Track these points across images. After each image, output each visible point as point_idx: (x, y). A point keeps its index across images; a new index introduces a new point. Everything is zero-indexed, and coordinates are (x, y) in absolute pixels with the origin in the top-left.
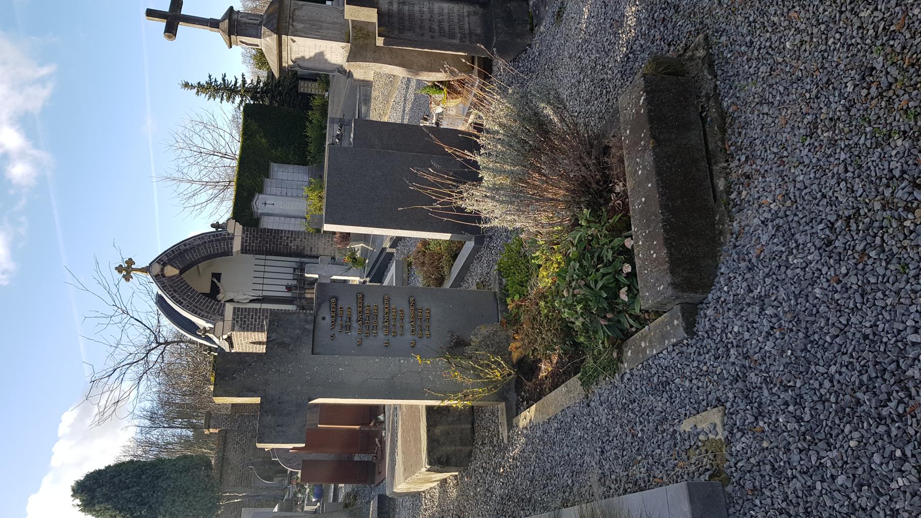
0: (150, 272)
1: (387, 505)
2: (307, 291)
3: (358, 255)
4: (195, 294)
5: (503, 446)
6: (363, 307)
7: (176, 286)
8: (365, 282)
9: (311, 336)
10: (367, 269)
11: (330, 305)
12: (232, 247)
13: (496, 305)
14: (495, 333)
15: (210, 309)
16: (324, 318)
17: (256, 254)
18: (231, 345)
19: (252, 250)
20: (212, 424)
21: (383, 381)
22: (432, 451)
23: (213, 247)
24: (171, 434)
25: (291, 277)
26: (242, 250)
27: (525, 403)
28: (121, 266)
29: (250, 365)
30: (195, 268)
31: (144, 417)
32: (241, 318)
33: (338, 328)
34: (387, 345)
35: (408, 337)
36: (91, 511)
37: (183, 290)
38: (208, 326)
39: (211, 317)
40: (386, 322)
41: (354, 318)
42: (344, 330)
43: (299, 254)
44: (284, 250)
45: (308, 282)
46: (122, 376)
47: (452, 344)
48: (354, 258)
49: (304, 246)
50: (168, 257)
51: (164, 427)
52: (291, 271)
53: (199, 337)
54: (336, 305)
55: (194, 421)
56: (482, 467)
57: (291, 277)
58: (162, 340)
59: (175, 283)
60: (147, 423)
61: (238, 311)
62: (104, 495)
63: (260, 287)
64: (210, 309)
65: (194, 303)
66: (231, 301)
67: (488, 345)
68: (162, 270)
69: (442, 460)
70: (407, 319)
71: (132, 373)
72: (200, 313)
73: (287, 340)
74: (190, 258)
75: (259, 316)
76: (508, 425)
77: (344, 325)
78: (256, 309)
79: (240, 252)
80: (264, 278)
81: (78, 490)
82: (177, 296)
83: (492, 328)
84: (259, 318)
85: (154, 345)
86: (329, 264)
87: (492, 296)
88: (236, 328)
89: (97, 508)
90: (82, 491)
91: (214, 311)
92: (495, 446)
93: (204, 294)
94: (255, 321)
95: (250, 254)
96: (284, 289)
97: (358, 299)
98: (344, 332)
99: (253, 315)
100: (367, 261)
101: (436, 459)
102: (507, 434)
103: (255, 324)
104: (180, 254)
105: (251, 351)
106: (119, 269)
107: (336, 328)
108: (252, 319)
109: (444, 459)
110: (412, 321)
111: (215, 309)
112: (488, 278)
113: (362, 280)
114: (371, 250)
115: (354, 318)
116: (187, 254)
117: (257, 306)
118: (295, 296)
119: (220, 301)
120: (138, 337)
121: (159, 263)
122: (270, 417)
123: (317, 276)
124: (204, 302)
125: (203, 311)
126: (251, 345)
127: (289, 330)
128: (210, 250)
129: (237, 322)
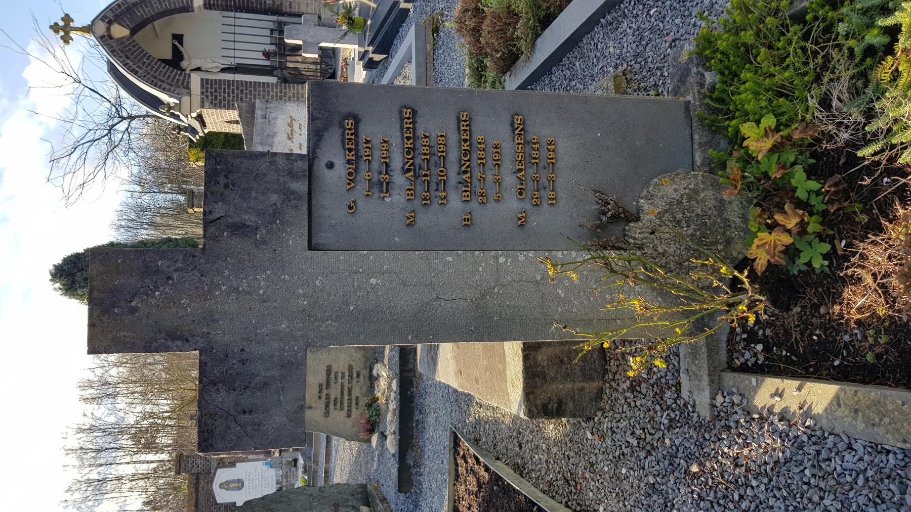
0: (93, 33)
1: (411, 361)
2: (289, 58)
5: (695, 419)
6: (415, 138)
8: (366, 52)
9: (305, 208)
10: (369, 35)
11: (343, 135)
13: (688, 132)
15: (172, 81)
16: (330, 166)
17: (223, 10)
18: (203, 124)
19: (218, 4)
24: (164, 199)
25: (268, 40)
26: (205, 4)
27: (760, 347)
28: (56, 24)
29: (169, 278)
30: (149, 27)
31: (133, 182)
32: (211, 93)
33: (362, 187)
34: (468, 223)
35: (512, 204)
36: (74, 295)
37: (137, 56)
38: (172, 101)
39: (174, 90)
40: (465, 172)
41: (397, 162)
42: (376, 190)
43: (275, 11)
45: (288, 48)
46: (84, 156)
47: (604, 219)
48: (350, 19)
50: (113, 12)
52: (268, 33)
53: (164, 114)
54: (356, 134)
55: (184, 186)
56: (633, 433)
57: (268, 40)
58: (125, 114)
59: (125, 47)
60: (138, 188)
61: (207, 84)
63: (231, 53)
64: (172, 81)
65: (152, 73)
66: (198, 69)
67: (679, 222)
68: (108, 29)
70: (508, 165)
71: (95, 152)
72: (161, 85)
73: (250, 218)
75: (233, 89)
76: (712, 382)
77: (375, 179)
78: (229, 81)
79: (202, 8)
80: (235, 26)
81: (56, 274)
82: (131, 64)
83: (685, 183)
84: (233, 92)
85: (116, 120)
86: (315, 25)
87: (683, 110)
88: (207, 104)
89: (79, 292)
90: (61, 276)
92: (668, 408)
93: (163, 61)
94: (229, 96)
95: (215, 9)
96: (260, 56)
97: (402, 120)
98: (376, 195)
99: (225, 89)
100: (369, 22)
102: (708, 401)
103: (229, 100)
104: (128, 9)
106: (55, 28)
107: (358, 187)
108: (224, 93)
110: (520, 170)
111: (178, 80)
112: (637, 66)
113: (362, 50)
114: (373, 8)
115: (397, 162)
116: (137, 8)
117: (229, 77)
118: (274, 64)
119: (185, 70)
120: (100, 111)
121: (103, 21)
122: (223, 393)
123: (300, 42)
124: (164, 71)
125: (163, 82)
126: (227, 125)
128: (166, 5)
129: (207, 96)
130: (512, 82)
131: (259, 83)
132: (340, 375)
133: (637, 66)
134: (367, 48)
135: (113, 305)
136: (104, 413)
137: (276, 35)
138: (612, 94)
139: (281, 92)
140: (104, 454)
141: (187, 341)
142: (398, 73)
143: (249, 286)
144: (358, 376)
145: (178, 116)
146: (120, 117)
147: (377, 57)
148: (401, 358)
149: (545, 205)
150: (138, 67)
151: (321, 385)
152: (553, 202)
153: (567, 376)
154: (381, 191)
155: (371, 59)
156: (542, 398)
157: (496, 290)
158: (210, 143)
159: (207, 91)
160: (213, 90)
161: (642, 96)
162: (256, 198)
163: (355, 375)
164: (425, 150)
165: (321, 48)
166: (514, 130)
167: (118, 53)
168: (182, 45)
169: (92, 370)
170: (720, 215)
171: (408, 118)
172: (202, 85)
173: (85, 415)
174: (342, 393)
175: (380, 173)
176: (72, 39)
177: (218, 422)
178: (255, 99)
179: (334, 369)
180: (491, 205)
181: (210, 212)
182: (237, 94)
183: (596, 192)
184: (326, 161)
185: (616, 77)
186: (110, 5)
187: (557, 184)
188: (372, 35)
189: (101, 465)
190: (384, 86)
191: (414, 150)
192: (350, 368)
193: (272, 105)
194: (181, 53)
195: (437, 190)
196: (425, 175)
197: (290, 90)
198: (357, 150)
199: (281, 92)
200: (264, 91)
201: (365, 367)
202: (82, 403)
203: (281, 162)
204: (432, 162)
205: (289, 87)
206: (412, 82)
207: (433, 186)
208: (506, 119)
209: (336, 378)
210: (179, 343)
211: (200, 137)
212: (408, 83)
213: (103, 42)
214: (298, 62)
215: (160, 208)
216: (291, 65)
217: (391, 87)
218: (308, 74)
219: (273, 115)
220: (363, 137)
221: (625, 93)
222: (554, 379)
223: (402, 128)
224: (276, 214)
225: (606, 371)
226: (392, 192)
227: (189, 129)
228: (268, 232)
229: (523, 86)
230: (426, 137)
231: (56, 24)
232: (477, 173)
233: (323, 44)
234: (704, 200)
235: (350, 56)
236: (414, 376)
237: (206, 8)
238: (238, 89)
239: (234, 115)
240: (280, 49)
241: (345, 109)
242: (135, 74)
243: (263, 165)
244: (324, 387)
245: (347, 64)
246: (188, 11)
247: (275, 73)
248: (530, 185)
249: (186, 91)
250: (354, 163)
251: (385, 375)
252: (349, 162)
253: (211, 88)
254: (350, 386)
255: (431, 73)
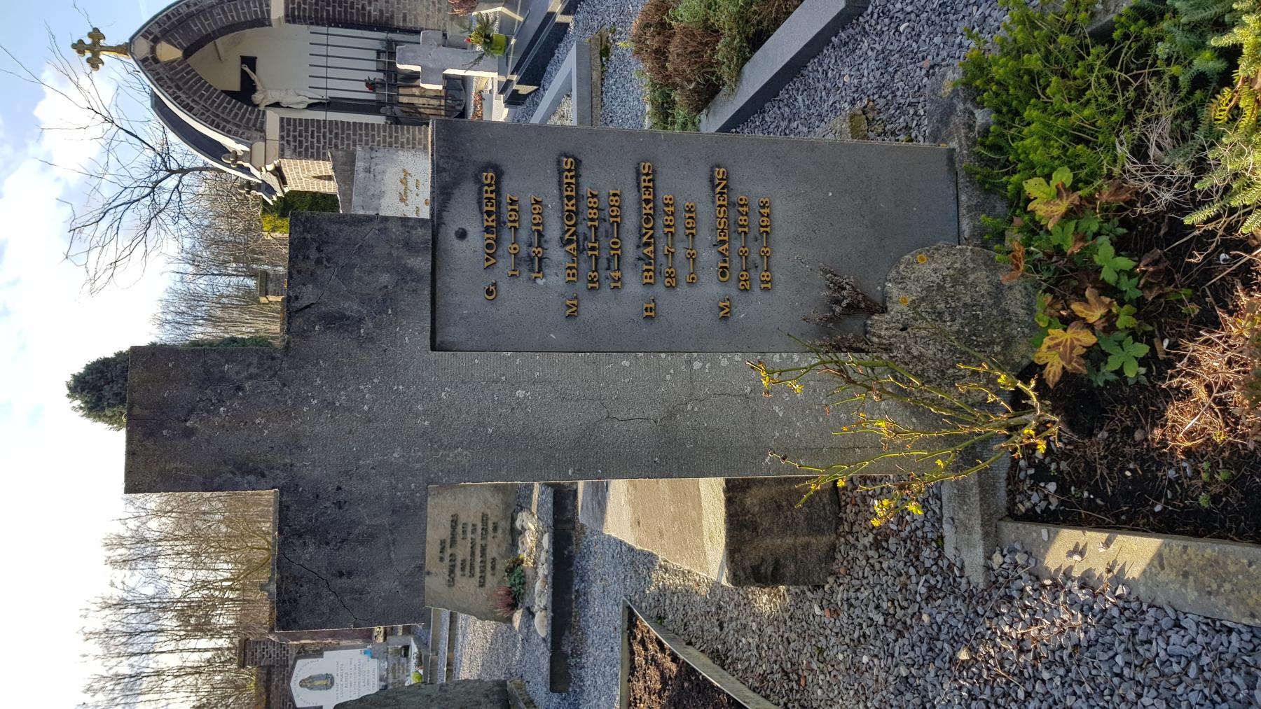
0: (132, 54)
1: (569, 508)
2: (401, 91)
3: (495, 31)
4: (213, 93)
6: (578, 197)
7: (180, 79)
8: (509, 82)
9: (427, 292)
10: (513, 59)
11: (480, 192)
12: (268, 12)
13: (952, 191)
14: (960, 276)
15: (241, 120)
16: (462, 235)
17: (312, 24)
18: (283, 180)
20: (270, 290)
21: (646, 425)
22: (739, 551)
23: (236, 8)
25: (373, 66)
26: (287, 16)
27: (1052, 487)
28: (81, 42)
29: (239, 388)
31: (184, 260)
32: (295, 137)
33: (505, 264)
34: (651, 314)
35: (711, 289)
37: (192, 86)
38: (240, 148)
39: (243, 133)
40: (647, 244)
41: (554, 231)
42: (524, 268)
43: (383, 25)
44: (358, 15)
46: (117, 223)
47: (838, 309)
48: (487, 36)
49: (392, 12)
50: (160, 26)
51: (213, 274)
52: (373, 55)
53: (228, 166)
54: (498, 191)
55: (255, 266)
56: (877, 607)
57: (373, 66)
58: (174, 166)
59: (177, 73)
60: (191, 269)
61: (289, 124)
62: (117, 395)
63: (322, 83)
64: (241, 120)
66: (277, 105)
67: (940, 314)
68: (153, 50)
69: (763, 569)
70: (705, 235)
71: (133, 219)
72: (224, 126)
73: (351, 307)
74: (199, 30)
76: (986, 535)
77: (523, 253)
78: (318, 121)
79: (283, 21)
80: (327, 67)
81: (76, 387)
82: (183, 97)
83: (948, 261)
84: (324, 137)
85: (162, 174)
86: (439, 45)
88: (288, 153)
89: (108, 413)
90: (83, 390)
91: (248, 122)
93: (228, 93)
94: (318, 142)
95: (300, 23)
96: (363, 87)
97: (560, 172)
98: (525, 275)
99: (313, 132)
100: (513, 41)
101: (749, 570)
102: (982, 561)
103: (318, 148)
104: (181, 22)
105: (316, 190)
106: (79, 47)
107: (501, 264)
108: (312, 137)
109: (767, 569)
110: (722, 242)
111: (249, 119)
112: (882, 102)
113: (503, 79)
114: (519, 22)
115: (554, 231)
116: (193, 20)
117: (319, 115)
118: (381, 98)
120: (139, 162)
122: (311, 548)
124: (230, 106)
125: (228, 122)
126: (316, 181)
127: (356, 272)
128: (232, 16)
129: (288, 142)
130: (711, 123)
131: (361, 124)
132: (470, 528)
133: (882, 102)
134: (509, 77)
135: (161, 426)
136: (140, 583)
137: (384, 58)
138: (848, 139)
139: (391, 137)
140: (138, 639)
141: (263, 476)
142: (552, 111)
143: (349, 399)
144: (495, 529)
145: (248, 169)
146: (167, 170)
147: (524, 89)
148: (555, 504)
149: (757, 290)
150: (194, 101)
151: (443, 542)
152: (768, 286)
153: (786, 528)
154: (532, 270)
155: (516, 91)
156: (752, 558)
157: (689, 407)
158: (292, 206)
159: (288, 135)
160: (297, 134)
161: (889, 141)
162: (360, 279)
163: (490, 528)
164: (592, 214)
165: (446, 77)
166: (714, 187)
167: (166, 82)
168: (254, 72)
169: (123, 521)
170: (997, 304)
171: (569, 171)
172: (282, 127)
173: (112, 584)
174: (473, 554)
175: (530, 245)
176: (103, 63)
177: (305, 588)
178: (355, 145)
179: (463, 518)
180: (683, 289)
181: (297, 298)
182: (330, 140)
183: (826, 272)
184: (456, 228)
185: (852, 117)
186: (156, 16)
187: (773, 261)
188: (518, 58)
189: (135, 655)
190: (535, 127)
191: (576, 214)
192: (485, 518)
193: (379, 154)
194: (253, 82)
195: (608, 269)
196: (593, 249)
197: (403, 134)
198: (498, 214)
199: (391, 137)
200: (367, 135)
201: (505, 517)
202: (109, 567)
203: (395, 230)
204: (602, 230)
205: (402, 130)
206: (572, 120)
207: (603, 263)
208: (704, 170)
209: (464, 532)
210: (252, 478)
211: (278, 198)
212: (567, 123)
213: (145, 66)
214: (413, 95)
215: (222, 296)
216: (404, 100)
217: (543, 129)
218: (428, 111)
219: (380, 168)
220: (506, 196)
221: (866, 137)
222: (769, 531)
223: (560, 183)
224: (385, 302)
225: (840, 521)
226: (547, 271)
227: (263, 188)
228: (377, 326)
229: (725, 128)
230: (593, 196)
231: (81, 42)
232: (663, 246)
233: (449, 72)
234: (974, 285)
235: (486, 87)
236: (574, 528)
237: (288, 21)
238: (331, 133)
239: (326, 167)
240: (389, 77)
241: (482, 158)
242: (190, 111)
243: (370, 233)
244: (448, 545)
245: (482, 99)
246: (263, 25)
247: (382, 110)
248: (736, 263)
249: (260, 134)
250: (494, 231)
251: (533, 528)
252: (488, 230)
253: (294, 131)
254: (483, 542)
255: (598, 111)
